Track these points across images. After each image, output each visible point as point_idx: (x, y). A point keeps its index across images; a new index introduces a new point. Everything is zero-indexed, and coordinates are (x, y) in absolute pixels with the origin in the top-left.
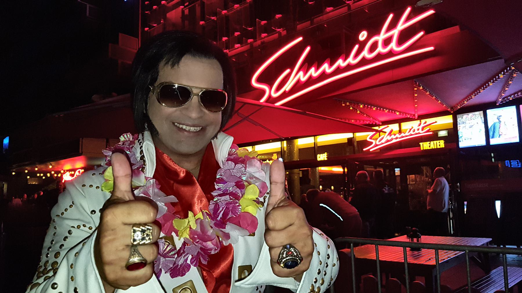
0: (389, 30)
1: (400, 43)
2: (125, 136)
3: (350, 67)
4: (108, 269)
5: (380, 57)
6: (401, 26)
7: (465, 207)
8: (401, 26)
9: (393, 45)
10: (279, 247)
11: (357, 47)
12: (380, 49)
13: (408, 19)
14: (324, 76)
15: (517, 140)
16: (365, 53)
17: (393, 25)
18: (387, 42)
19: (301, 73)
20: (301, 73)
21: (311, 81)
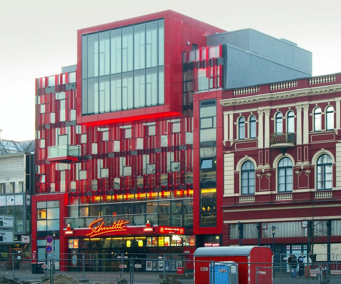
0: (119, 224)
1: (121, 227)
2: (191, 215)
3: (112, 230)
4: (219, 266)
5: (117, 229)
6: (121, 224)
7: (161, 169)
8: (121, 224)
9: (120, 227)
10: (276, 225)
11: (114, 225)
12: (118, 227)
13: (122, 223)
14: (107, 230)
15: (211, 167)
16: (115, 227)
17: (120, 223)
18: (119, 226)
19: (102, 228)
20: (102, 228)
21: (104, 231)
